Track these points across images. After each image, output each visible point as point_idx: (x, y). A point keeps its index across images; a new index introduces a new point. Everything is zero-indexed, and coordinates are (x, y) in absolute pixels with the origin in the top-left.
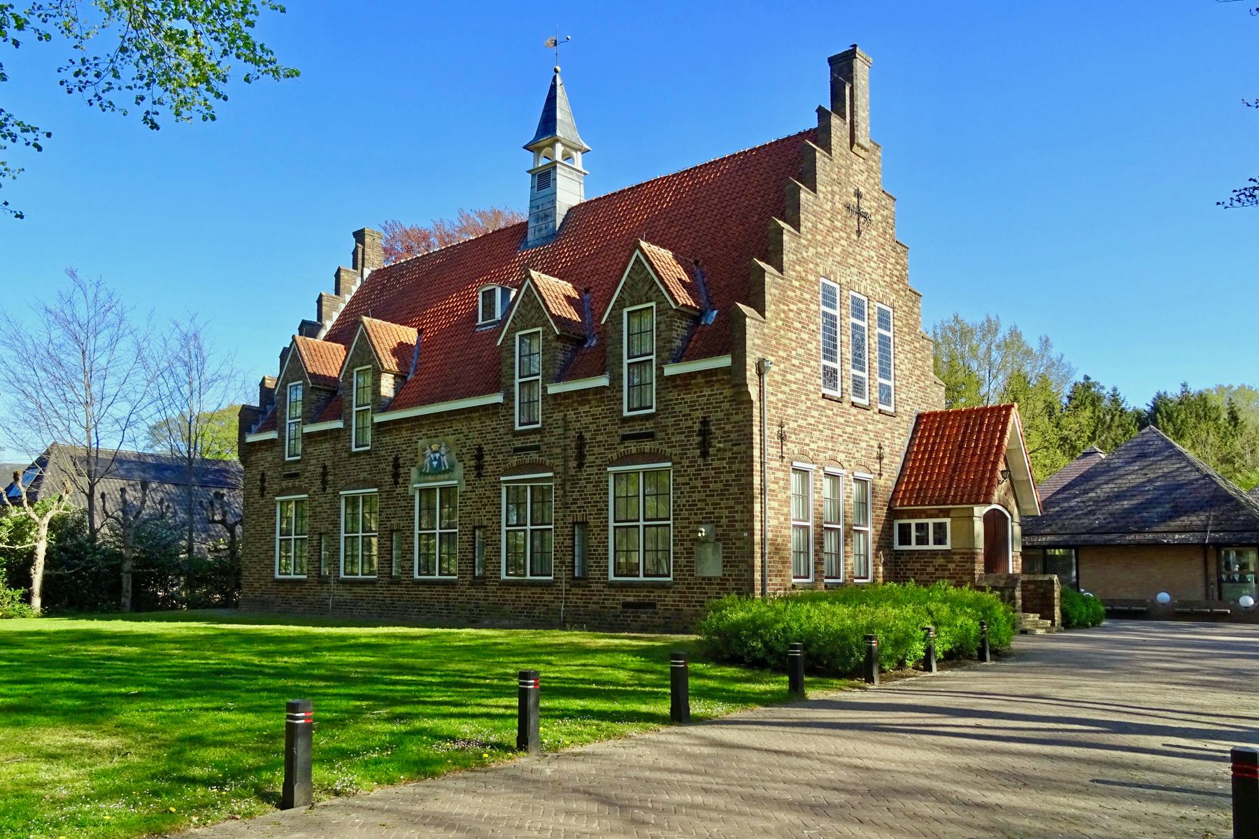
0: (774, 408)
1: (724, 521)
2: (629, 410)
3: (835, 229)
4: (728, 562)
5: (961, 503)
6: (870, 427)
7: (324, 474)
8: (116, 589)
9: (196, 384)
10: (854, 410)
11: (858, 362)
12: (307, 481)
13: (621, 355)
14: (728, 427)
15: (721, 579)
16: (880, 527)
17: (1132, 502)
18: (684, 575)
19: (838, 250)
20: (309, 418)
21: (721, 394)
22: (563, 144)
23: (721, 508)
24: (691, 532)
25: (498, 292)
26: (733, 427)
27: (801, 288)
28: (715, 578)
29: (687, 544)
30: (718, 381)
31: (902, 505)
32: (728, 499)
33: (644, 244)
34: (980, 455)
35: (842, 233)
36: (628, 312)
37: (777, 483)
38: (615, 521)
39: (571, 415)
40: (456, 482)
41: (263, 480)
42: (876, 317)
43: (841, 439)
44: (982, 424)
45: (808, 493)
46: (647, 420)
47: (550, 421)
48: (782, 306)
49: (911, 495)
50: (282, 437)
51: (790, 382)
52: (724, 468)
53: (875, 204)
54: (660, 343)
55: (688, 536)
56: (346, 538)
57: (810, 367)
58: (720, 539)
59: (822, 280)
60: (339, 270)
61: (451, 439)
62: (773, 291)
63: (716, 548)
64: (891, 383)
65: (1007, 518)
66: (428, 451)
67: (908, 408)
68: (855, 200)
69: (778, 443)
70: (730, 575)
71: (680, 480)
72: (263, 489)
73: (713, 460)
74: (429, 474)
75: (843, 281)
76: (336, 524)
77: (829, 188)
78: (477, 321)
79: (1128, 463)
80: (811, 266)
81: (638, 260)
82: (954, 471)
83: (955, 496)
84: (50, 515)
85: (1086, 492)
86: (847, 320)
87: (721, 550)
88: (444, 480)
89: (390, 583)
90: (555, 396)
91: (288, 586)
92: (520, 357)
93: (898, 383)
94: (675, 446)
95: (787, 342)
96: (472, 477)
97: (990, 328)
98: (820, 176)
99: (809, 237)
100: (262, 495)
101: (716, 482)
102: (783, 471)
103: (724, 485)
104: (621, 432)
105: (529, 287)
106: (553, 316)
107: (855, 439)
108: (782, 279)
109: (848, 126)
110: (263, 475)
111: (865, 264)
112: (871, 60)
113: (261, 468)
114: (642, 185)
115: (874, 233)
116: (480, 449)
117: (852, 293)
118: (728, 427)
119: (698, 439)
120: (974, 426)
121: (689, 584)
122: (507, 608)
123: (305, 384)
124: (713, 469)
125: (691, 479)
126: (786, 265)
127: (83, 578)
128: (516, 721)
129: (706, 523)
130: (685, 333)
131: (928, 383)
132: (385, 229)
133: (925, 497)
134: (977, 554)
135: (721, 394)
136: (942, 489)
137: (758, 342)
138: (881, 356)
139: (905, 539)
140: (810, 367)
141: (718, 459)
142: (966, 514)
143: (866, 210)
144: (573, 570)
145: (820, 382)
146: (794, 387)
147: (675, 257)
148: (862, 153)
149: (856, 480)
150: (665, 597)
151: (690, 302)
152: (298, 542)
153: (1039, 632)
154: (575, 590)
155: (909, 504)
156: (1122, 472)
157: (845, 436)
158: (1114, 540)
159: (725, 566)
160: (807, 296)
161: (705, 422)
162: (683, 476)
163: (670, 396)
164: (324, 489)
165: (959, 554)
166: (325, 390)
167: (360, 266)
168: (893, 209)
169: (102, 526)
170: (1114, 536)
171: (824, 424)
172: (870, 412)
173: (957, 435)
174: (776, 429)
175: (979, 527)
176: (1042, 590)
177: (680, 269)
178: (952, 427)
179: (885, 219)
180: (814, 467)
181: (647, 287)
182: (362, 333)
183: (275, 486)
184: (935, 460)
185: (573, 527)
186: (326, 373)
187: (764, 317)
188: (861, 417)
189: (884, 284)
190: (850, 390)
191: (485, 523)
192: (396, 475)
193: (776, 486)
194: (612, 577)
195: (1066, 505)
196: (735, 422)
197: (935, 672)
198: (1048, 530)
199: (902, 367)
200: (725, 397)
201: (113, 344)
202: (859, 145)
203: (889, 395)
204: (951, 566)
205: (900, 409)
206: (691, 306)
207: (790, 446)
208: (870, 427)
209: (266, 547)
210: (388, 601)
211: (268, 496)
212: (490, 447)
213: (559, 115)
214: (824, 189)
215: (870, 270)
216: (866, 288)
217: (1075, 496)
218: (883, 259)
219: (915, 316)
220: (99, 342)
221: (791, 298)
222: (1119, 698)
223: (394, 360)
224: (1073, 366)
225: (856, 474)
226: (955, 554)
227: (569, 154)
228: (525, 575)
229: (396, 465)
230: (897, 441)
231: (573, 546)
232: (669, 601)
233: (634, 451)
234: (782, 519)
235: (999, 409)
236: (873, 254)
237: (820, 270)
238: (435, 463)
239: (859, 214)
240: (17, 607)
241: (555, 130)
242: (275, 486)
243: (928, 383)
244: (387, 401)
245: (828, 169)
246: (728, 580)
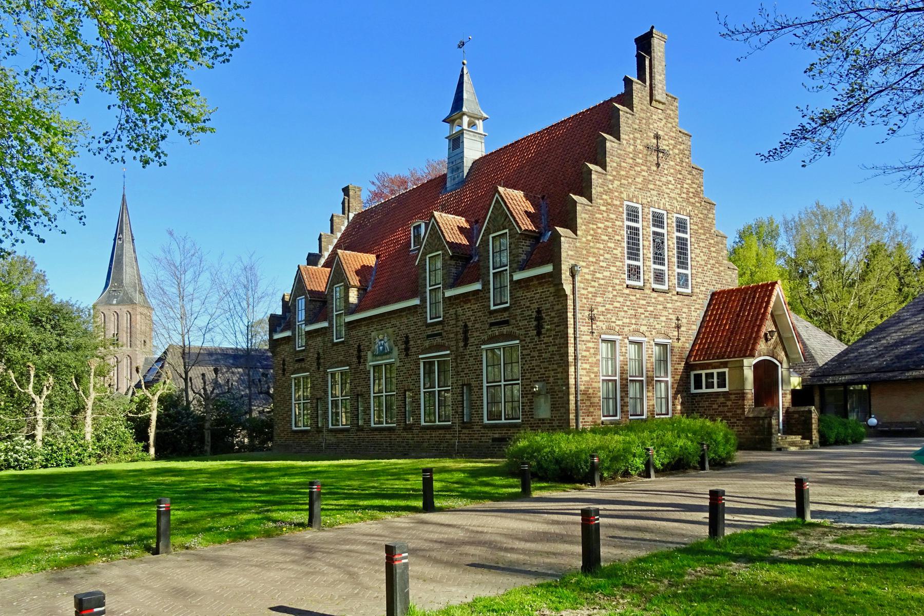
0: (585, 298)
1: (551, 380)
2: (495, 305)
3: (637, 165)
4: (554, 407)
5: (734, 357)
6: (669, 305)
7: (318, 359)
8: (202, 440)
9: (251, 300)
10: (654, 294)
11: (659, 258)
13: (489, 267)
14: (553, 314)
15: (550, 420)
16: (678, 377)
17: (913, 346)
19: (639, 180)
20: (308, 322)
21: (548, 291)
22: (468, 116)
23: (549, 371)
25: (423, 226)
27: (607, 211)
28: (546, 419)
29: (530, 396)
30: (546, 282)
31: (695, 360)
32: (553, 364)
33: (501, 189)
34: (751, 321)
35: (643, 167)
36: (493, 237)
37: (589, 351)
38: (487, 383)
39: (460, 311)
40: (393, 360)
41: (284, 364)
42: (674, 225)
43: (643, 316)
44: (754, 297)
45: (616, 357)
47: (447, 315)
48: (591, 226)
49: (701, 352)
50: (294, 334)
51: (599, 278)
53: (673, 142)
54: (512, 258)
56: (425, 392)
57: (616, 266)
58: (551, 392)
59: (626, 203)
60: (332, 216)
61: (390, 330)
62: (583, 215)
64: (688, 272)
65: (778, 366)
66: (377, 340)
67: (704, 289)
68: (655, 141)
69: (589, 323)
71: (525, 352)
72: (284, 370)
74: (378, 355)
75: (644, 201)
77: (631, 136)
79: (914, 315)
80: (616, 194)
81: (497, 201)
82: (732, 333)
83: (731, 352)
84: (158, 394)
85: (879, 340)
86: (648, 229)
87: (549, 400)
88: (387, 359)
89: (358, 430)
90: (450, 298)
91: (300, 435)
92: (430, 271)
93: (694, 271)
95: (596, 251)
96: (403, 356)
97: (845, 209)
98: (624, 128)
99: (614, 173)
100: (284, 374)
101: (546, 352)
102: (593, 342)
103: (551, 355)
104: (490, 321)
105: (433, 223)
106: (448, 242)
107: (655, 315)
108: (591, 206)
109: (648, 88)
110: (284, 361)
111: (664, 187)
112: (666, 36)
113: (283, 356)
114: (518, 141)
115: (672, 163)
116: (407, 337)
117: (652, 209)
118: (553, 314)
119: (535, 323)
120: (749, 299)
122: (426, 445)
123: (306, 298)
126: (594, 196)
127: (180, 434)
128: (308, 513)
129: (541, 381)
130: (529, 249)
131: (721, 269)
132: (378, 179)
133: (711, 353)
134: (747, 393)
135: (548, 291)
136: (722, 347)
137: (571, 253)
138: (679, 253)
139: (698, 385)
140: (616, 266)
142: (738, 365)
143: (665, 147)
144: (463, 417)
145: (626, 276)
147: (526, 196)
148: (661, 106)
149: (656, 344)
151: (532, 227)
152: (297, 405)
153: (793, 449)
154: (464, 431)
155: (699, 360)
156: (909, 323)
157: (647, 314)
158: (896, 376)
159: (552, 411)
161: (539, 311)
162: (526, 349)
163: (518, 295)
164: (319, 368)
165: (734, 394)
166: (319, 301)
167: (346, 212)
168: (689, 143)
169: (194, 399)
170: (896, 373)
171: (628, 306)
172: (670, 295)
173: (737, 306)
174: (587, 313)
175: (749, 374)
176: (803, 418)
177: (528, 204)
178: (734, 301)
179: (682, 152)
180: (620, 337)
181: (503, 219)
182: (338, 261)
183: (291, 368)
184: (721, 325)
185: (463, 388)
186: (319, 289)
187: (576, 235)
188: (661, 299)
189: (681, 200)
190: (652, 280)
191: (411, 387)
192: (359, 357)
193: (588, 353)
194: (486, 421)
195: (863, 350)
196: (557, 310)
197: (653, 478)
198: (847, 371)
199: (698, 259)
200: (551, 293)
201: (195, 278)
202: (656, 101)
203: (687, 280)
204: (729, 403)
205: (696, 290)
206: (531, 231)
207: (600, 325)
208: (669, 305)
209: (287, 409)
210: (357, 442)
211: (287, 375)
212: (413, 335)
213: (465, 96)
214: (627, 137)
215: (668, 191)
216: (664, 204)
217: (871, 343)
218: (681, 182)
219: (709, 220)
220: (187, 277)
221: (600, 219)
222: (732, 490)
223: (358, 278)
224: (914, 235)
225: (656, 340)
226: (731, 394)
227: (474, 122)
228: (435, 422)
229: (359, 351)
230: (693, 314)
231: (463, 401)
233: (497, 334)
234: (593, 376)
235: (767, 285)
236: (671, 179)
237: (624, 196)
238: (381, 348)
239: (658, 150)
240: (140, 454)
241: (462, 107)
242: (291, 368)
243: (721, 269)
244: (354, 307)
245: (630, 122)
246: (554, 420)
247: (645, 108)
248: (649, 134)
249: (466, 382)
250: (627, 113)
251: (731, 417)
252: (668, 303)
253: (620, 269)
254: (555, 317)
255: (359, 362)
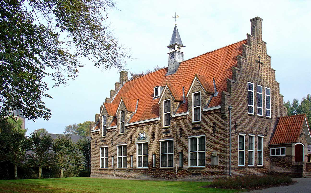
0: (233, 119)
4: (220, 161)
7: (112, 140)
12: (108, 142)
14: (221, 125)
18: (209, 165)
19: (253, 74)
21: (219, 116)
22: (177, 45)
23: (218, 147)
24: (210, 154)
26: (222, 125)
30: (217, 112)
37: (234, 140)
46: (199, 124)
51: (238, 111)
52: (219, 136)
55: (210, 155)
62: (233, 87)
63: (217, 158)
65: (303, 146)
68: (258, 59)
70: (221, 165)
71: (207, 140)
73: (216, 134)
76: (116, 154)
78: (153, 97)
80: (245, 79)
87: (218, 158)
91: (104, 171)
94: (206, 131)
100: (96, 146)
101: (217, 140)
102: (236, 136)
103: (219, 141)
108: (236, 83)
110: (96, 141)
113: (96, 139)
115: (264, 68)
116: (154, 133)
117: (257, 85)
118: (221, 125)
119: (213, 128)
121: (210, 168)
124: (216, 136)
125: (210, 139)
131: (281, 109)
141: (218, 134)
144: (179, 165)
146: (239, 113)
150: (204, 171)
160: (243, 87)
161: (214, 124)
164: (112, 145)
165: (288, 157)
174: (234, 125)
188: (260, 120)
192: (131, 140)
193: (234, 140)
205: (273, 117)
208: (263, 122)
216: (262, 83)
221: (239, 88)
226: (287, 157)
229: (131, 138)
231: (179, 159)
232: (204, 172)
233: (195, 132)
234: (235, 149)
236: (264, 73)
237: (248, 79)
238: (142, 137)
239: (260, 62)
247: (255, 46)
248: (256, 56)
249: (181, 151)
250: (249, 48)
251: (286, 166)
252: (263, 121)
253: (246, 108)
254: (221, 126)
255: (131, 142)
